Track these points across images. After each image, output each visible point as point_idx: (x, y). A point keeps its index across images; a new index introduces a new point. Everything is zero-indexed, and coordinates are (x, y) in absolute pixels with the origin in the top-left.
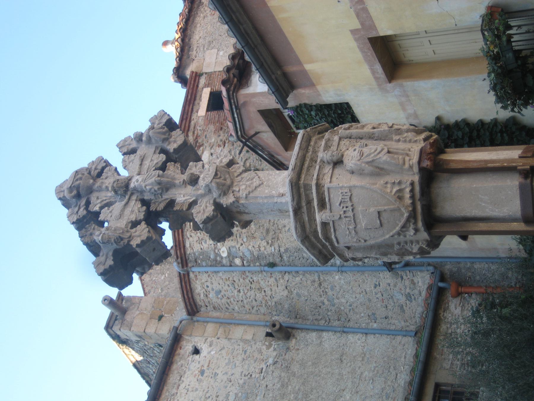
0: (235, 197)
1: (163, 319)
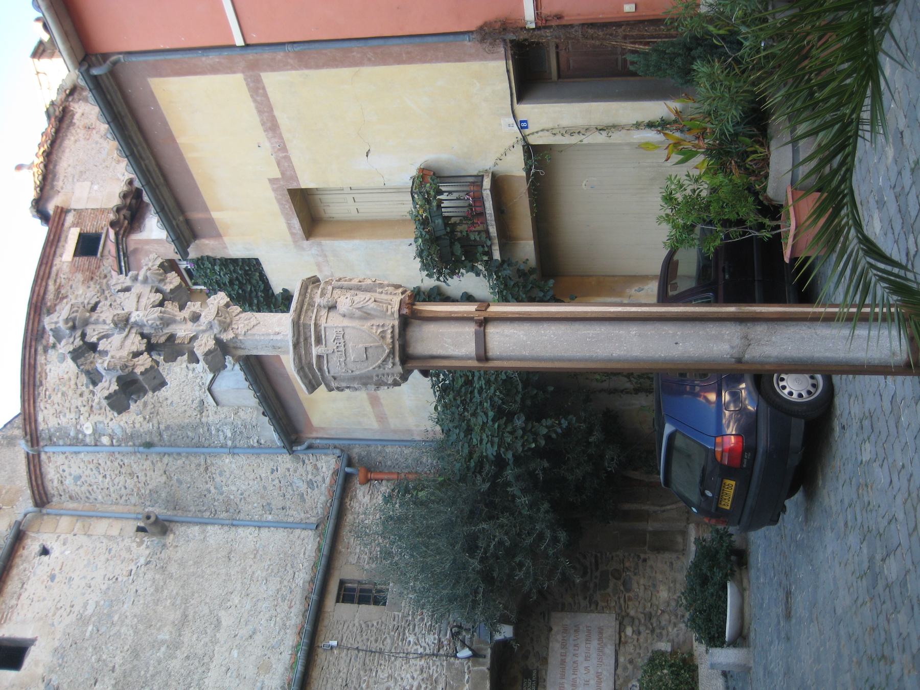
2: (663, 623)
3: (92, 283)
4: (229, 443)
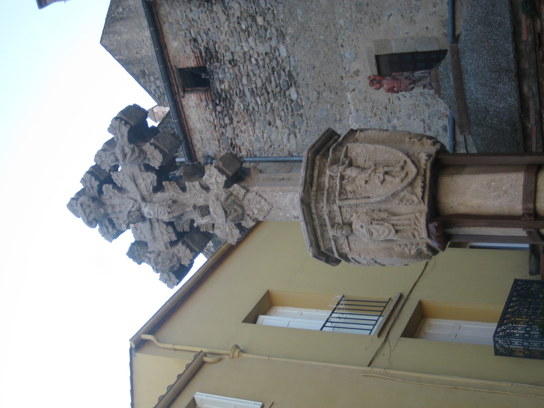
0: (253, 220)
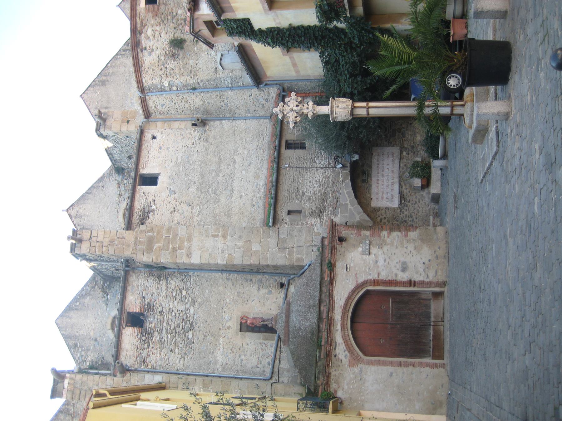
1: (130, 122)
2: (419, 150)
3: (157, 18)
4: (230, 85)
